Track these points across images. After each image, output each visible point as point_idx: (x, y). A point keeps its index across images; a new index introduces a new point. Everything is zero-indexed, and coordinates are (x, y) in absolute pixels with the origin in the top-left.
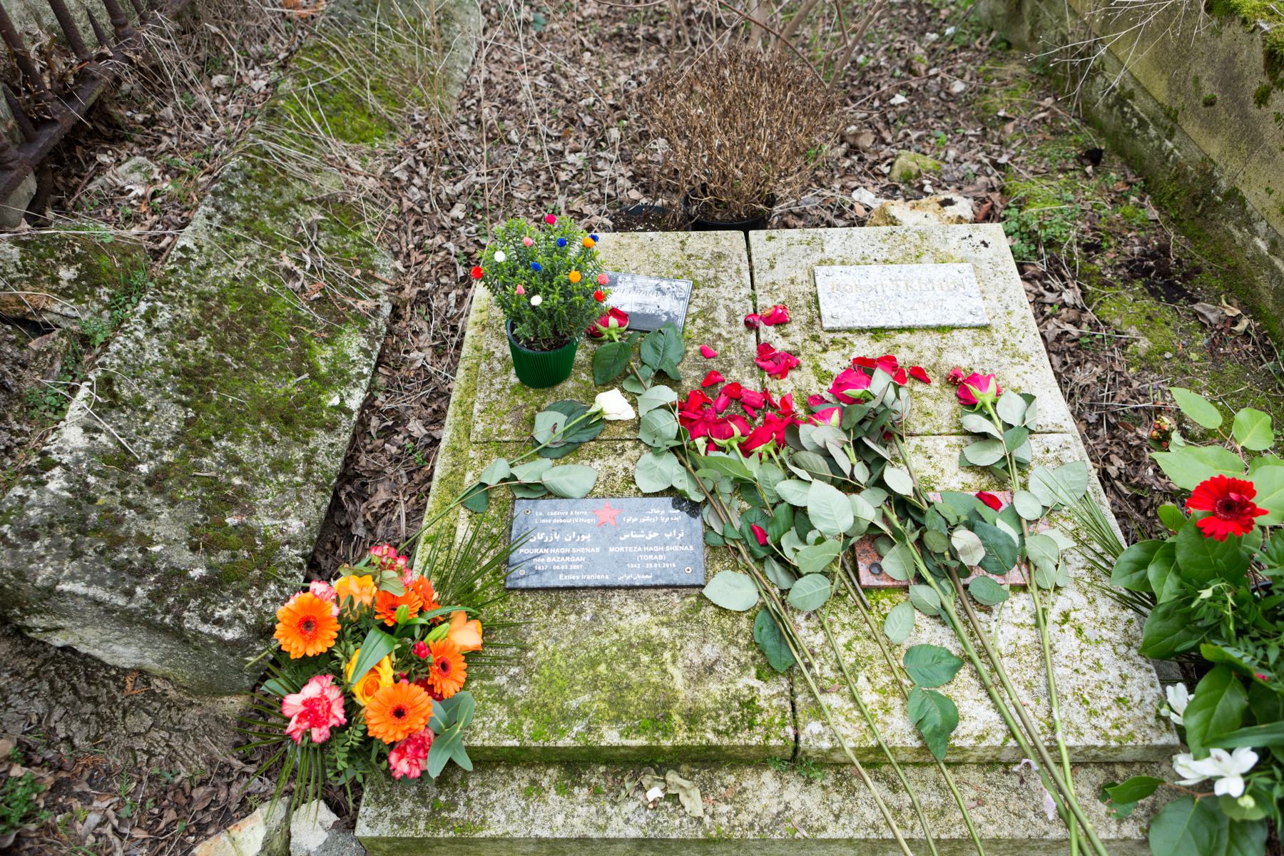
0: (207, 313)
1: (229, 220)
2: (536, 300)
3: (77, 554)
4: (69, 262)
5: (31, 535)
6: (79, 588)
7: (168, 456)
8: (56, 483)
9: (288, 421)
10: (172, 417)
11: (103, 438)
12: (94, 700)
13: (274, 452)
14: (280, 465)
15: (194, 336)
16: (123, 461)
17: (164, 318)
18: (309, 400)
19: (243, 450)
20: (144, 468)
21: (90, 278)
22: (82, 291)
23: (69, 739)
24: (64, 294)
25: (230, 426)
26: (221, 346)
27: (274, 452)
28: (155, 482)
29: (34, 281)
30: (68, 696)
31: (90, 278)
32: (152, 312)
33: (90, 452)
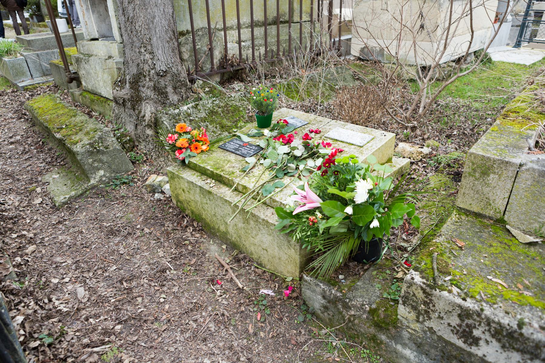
0: (225, 106)
1: (245, 96)
2: (255, 98)
3: (170, 120)
4: (209, 87)
5: (167, 114)
6: (166, 123)
7: (197, 119)
8: (177, 111)
9: (222, 127)
10: (203, 115)
11: (189, 111)
12: (159, 152)
13: (215, 129)
14: (213, 132)
15: (219, 108)
16: (189, 115)
17: (217, 102)
18: (231, 128)
19: (210, 126)
20: (191, 118)
21: (210, 92)
22: (208, 94)
23: (152, 156)
24: (204, 93)
25: (212, 122)
26: (223, 112)
27: (215, 129)
28: (191, 121)
29: (201, 88)
30: (157, 149)
31: (210, 92)
32: (215, 101)
33: (186, 111)
